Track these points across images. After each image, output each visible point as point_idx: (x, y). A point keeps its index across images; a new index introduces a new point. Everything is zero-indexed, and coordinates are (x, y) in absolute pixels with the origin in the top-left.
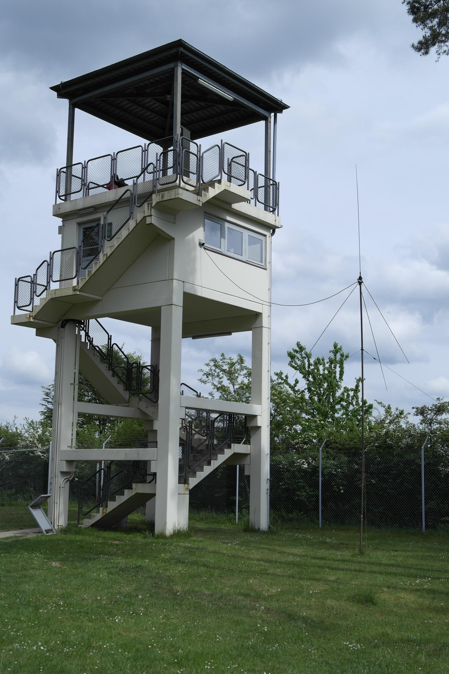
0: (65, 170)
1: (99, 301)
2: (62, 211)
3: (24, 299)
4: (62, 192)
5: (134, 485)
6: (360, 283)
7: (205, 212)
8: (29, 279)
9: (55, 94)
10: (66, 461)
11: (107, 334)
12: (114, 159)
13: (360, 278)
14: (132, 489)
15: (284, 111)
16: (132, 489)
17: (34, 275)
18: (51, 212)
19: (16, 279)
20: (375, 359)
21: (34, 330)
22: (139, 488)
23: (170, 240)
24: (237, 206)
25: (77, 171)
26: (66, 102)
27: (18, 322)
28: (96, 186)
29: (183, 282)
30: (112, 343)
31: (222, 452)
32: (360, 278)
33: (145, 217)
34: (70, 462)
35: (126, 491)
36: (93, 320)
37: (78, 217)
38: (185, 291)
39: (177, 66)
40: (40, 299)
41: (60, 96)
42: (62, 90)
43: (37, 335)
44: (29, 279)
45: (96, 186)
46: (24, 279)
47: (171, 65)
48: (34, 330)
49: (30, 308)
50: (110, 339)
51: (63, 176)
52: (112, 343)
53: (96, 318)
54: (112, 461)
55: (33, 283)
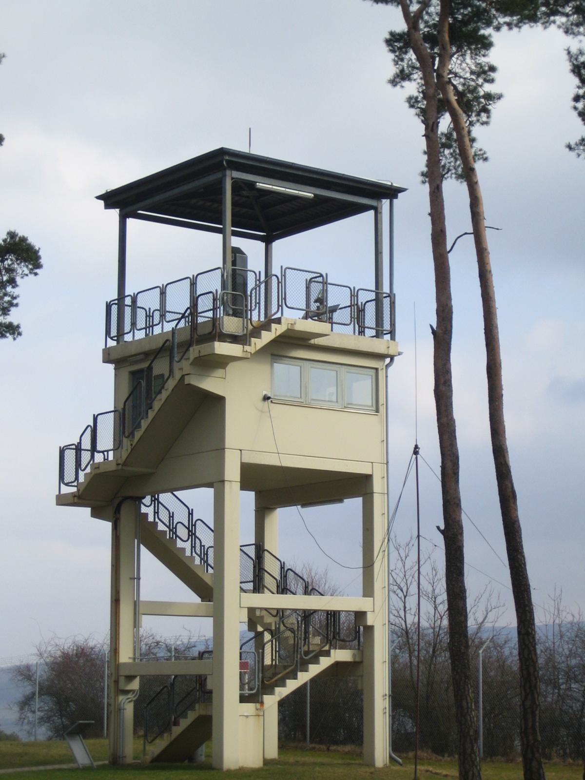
1: (152, 474)
2: (114, 356)
3: (69, 476)
4: (114, 332)
7: (272, 355)
8: (74, 447)
11: (166, 511)
12: (163, 293)
13: (416, 447)
14: (195, 710)
15: (400, 195)
17: (78, 443)
18: (100, 356)
19: (306, 280)
20: (435, 546)
21: (89, 509)
24: (312, 341)
26: (115, 213)
27: (62, 500)
30: (175, 522)
32: (416, 447)
33: (183, 376)
35: (189, 713)
36: (375, 333)
37: (131, 365)
38: (243, 461)
39: (225, 176)
41: (108, 206)
42: (111, 199)
46: (315, 279)
48: (89, 509)
49: (75, 484)
51: (114, 309)
52: (175, 522)
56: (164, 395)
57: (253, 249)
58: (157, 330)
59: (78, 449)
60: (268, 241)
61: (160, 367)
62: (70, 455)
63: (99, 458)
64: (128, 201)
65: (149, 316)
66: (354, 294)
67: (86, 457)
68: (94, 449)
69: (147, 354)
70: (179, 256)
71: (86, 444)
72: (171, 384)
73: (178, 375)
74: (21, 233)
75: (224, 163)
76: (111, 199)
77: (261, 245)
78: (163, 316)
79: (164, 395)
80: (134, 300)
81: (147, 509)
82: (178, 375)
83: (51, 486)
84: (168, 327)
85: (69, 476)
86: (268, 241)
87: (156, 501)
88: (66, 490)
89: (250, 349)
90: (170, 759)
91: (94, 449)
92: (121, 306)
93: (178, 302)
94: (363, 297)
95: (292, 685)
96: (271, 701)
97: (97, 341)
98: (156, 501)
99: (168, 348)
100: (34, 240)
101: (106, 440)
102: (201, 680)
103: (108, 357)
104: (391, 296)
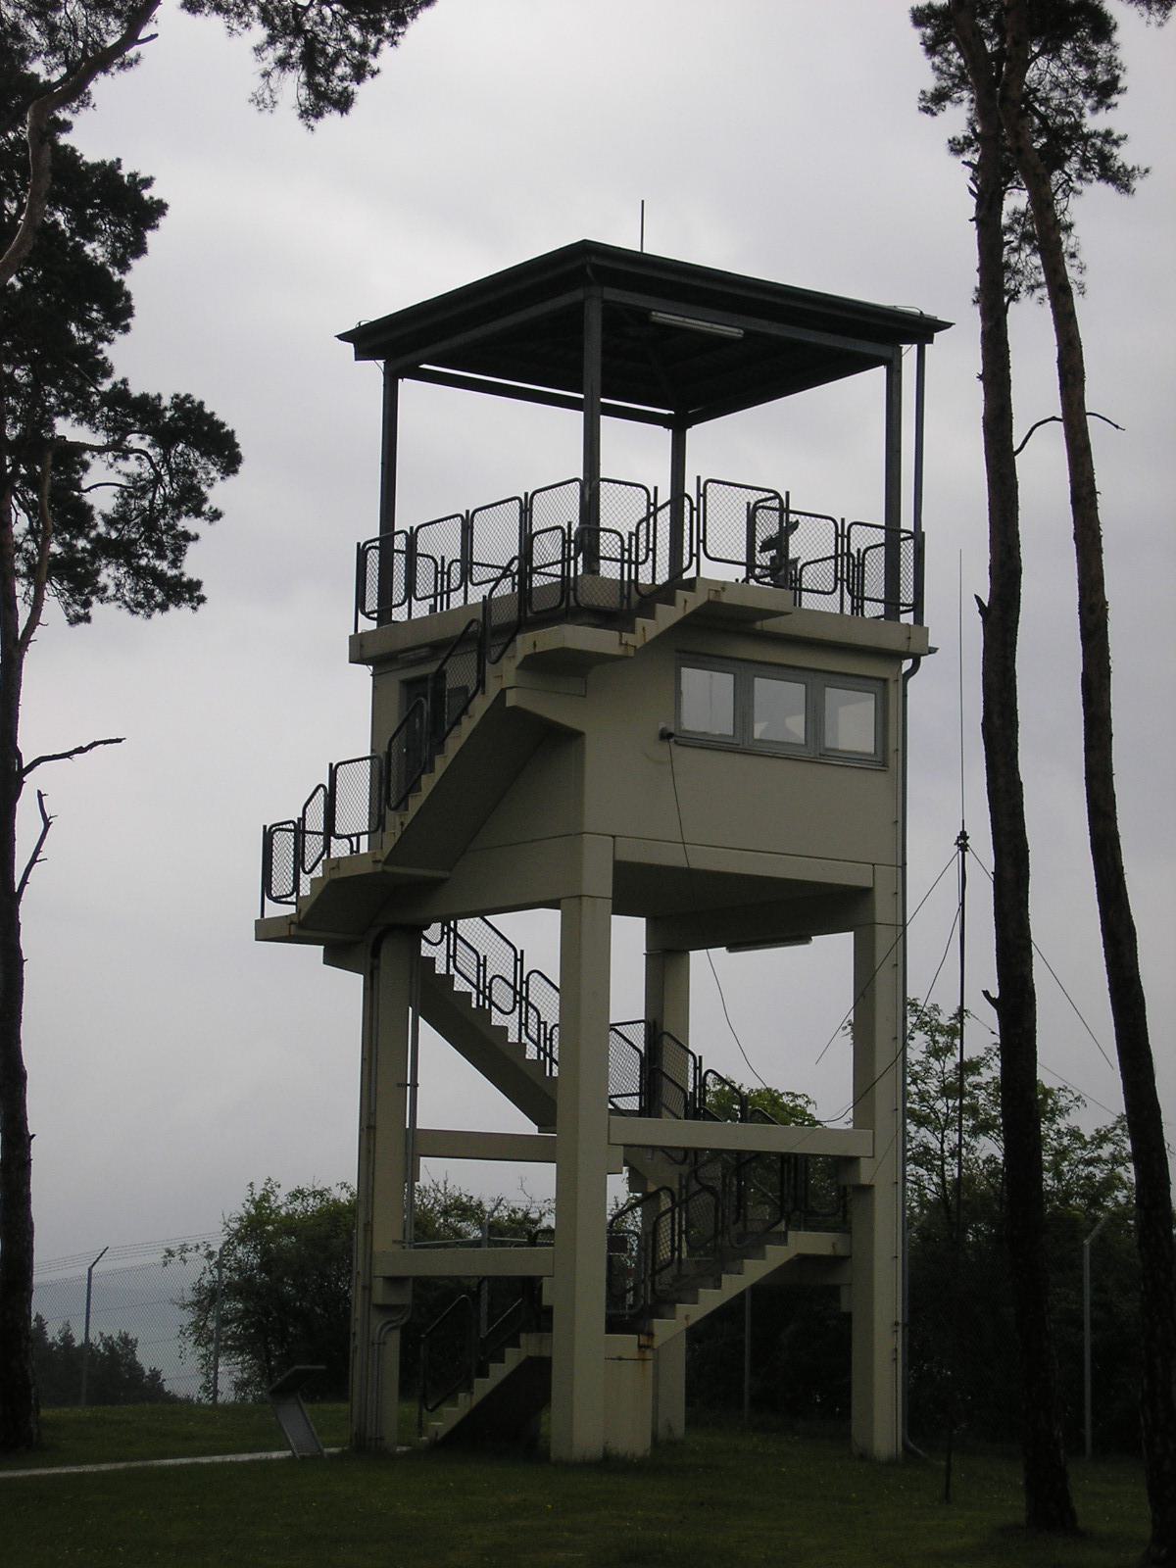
0: (377, 544)
1: (443, 881)
5: (523, 1338)
6: (964, 848)
9: (349, 348)
10: (384, 1277)
13: (963, 836)
14: (518, 1346)
16: (518, 1346)
22: (529, 1345)
23: (571, 737)
25: (400, 542)
26: (375, 369)
27: (268, 931)
28: (492, 584)
29: (614, 837)
31: (483, 1373)
32: (963, 836)
34: (394, 1281)
38: (618, 858)
40: (312, 880)
42: (367, 340)
43: (324, 963)
44: (291, 826)
45: (492, 584)
47: (578, 295)
49: (293, 899)
50: (519, 959)
51: (373, 557)
53: (481, 914)
54: (484, 1278)
55: (300, 830)
56: (468, 726)
58: (456, 600)
59: (300, 830)
60: (678, 427)
61: (460, 672)
62: (284, 843)
64: (404, 344)
65: (441, 572)
66: (842, 534)
67: (313, 845)
70: (498, 454)
71: (316, 821)
72: (480, 706)
73: (493, 689)
76: (367, 340)
77: (666, 435)
78: (466, 574)
79: (468, 726)
80: (412, 538)
82: (493, 689)
83: (247, 904)
85: (282, 883)
86: (678, 427)
87: (451, 933)
88: (274, 910)
89: (635, 640)
92: (387, 556)
93: (497, 544)
94: (860, 540)
95: (710, 1300)
96: (670, 1330)
97: (338, 618)
98: (451, 933)
99: (483, 634)
101: (355, 813)
104: (918, 537)
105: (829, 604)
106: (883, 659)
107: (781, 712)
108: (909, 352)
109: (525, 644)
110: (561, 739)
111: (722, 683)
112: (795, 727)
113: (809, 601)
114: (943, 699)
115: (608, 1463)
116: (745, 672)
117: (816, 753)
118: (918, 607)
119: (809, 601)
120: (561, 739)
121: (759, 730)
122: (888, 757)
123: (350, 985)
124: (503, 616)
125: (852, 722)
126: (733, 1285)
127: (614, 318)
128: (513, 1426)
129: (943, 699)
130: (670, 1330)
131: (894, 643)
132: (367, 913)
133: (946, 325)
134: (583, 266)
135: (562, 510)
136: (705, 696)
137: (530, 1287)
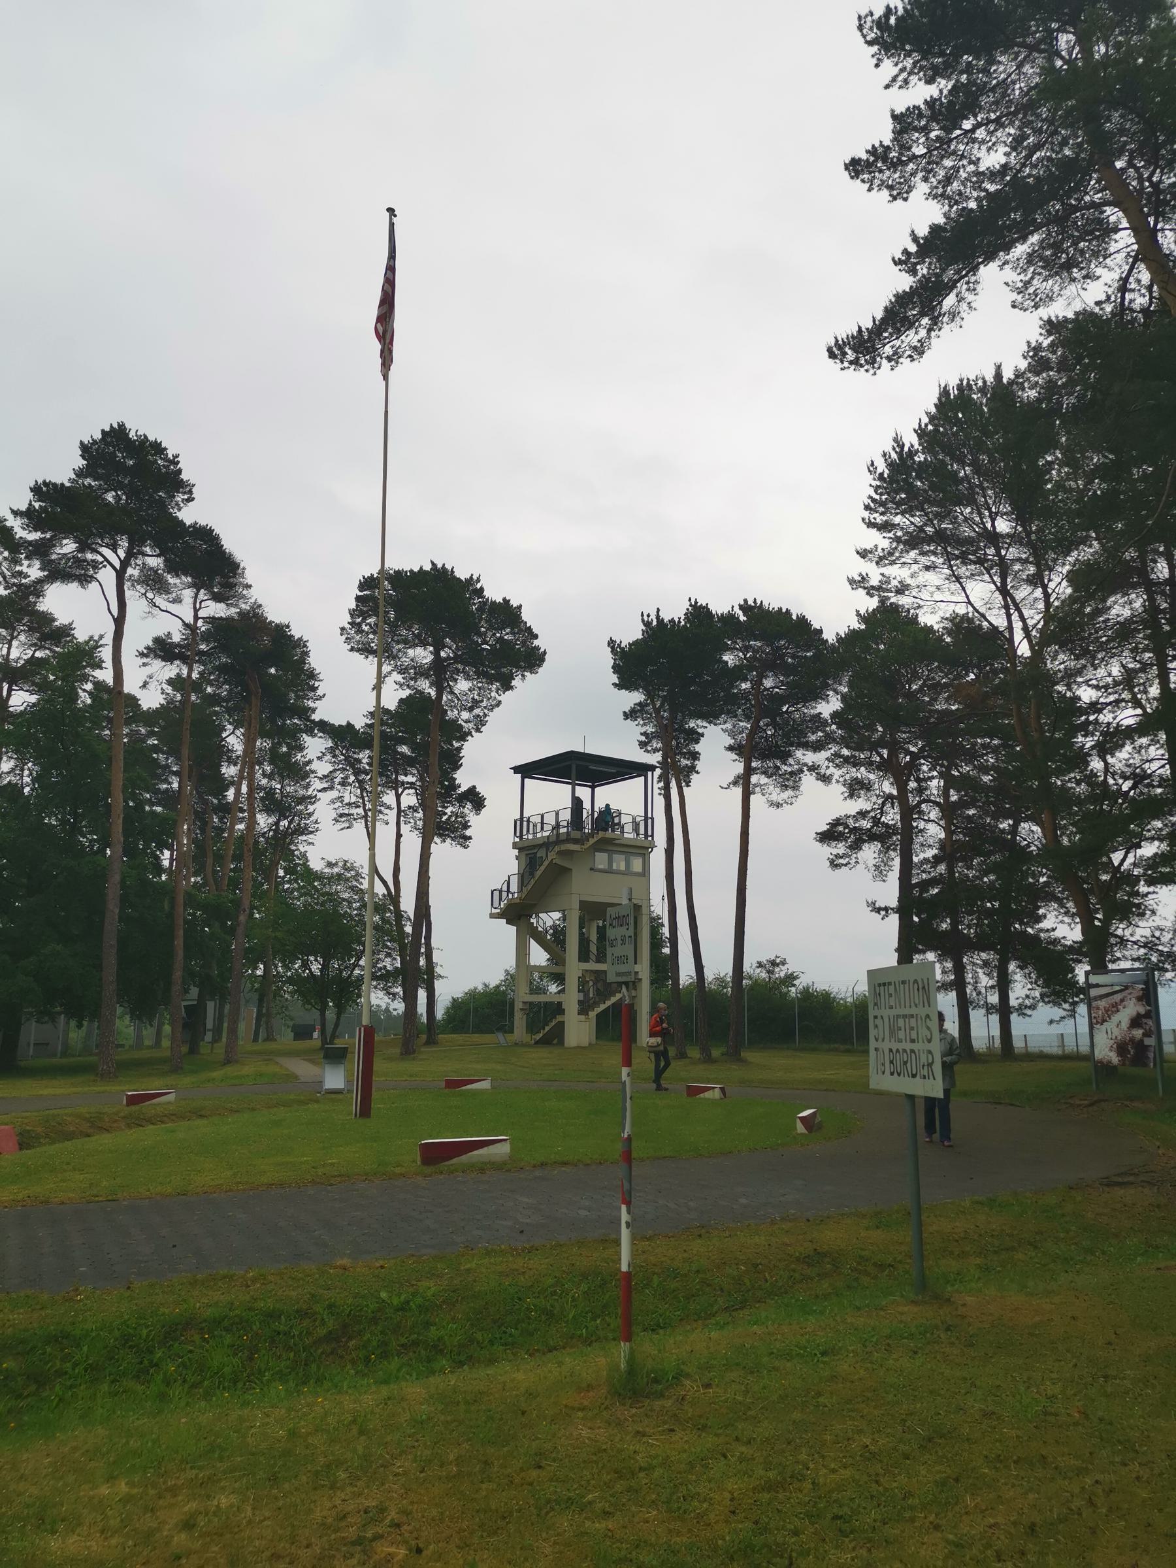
3: (496, 904)
22: (559, 1018)
27: (492, 916)
42: (517, 770)
56: (543, 868)
57: (583, 793)
58: (539, 835)
59: (501, 891)
60: (593, 788)
61: (541, 853)
62: (496, 894)
63: (510, 896)
64: (526, 771)
65: (535, 826)
66: (634, 818)
67: (504, 895)
68: (508, 891)
69: (534, 847)
70: (551, 800)
71: (505, 888)
72: (546, 863)
73: (550, 858)
74: (702, 602)
75: (1083, 718)
76: (517, 770)
77: (590, 790)
78: (542, 828)
79: (543, 868)
80: (528, 821)
81: (533, 921)
82: (550, 858)
83: (488, 909)
84: (546, 834)
85: (496, 904)
86: (593, 788)
87: (537, 916)
88: (494, 911)
89: (586, 846)
90: (546, 1042)
91: (508, 891)
92: (522, 822)
93: (550, 820)
94: (638, 819)
95: (603, 1007)
96: (592, 1014)
97: (510, 838)
98: (537, 916)
99: (547, 844)
100: (859, 377)
101: (514, 887)
102: (560, 1004)
103: (515, 846)
104: (652, 819)
105: (631, 836)
106: (643, 850)
107: (620, 863)
108: (650, 773)
109: (557, 849)
110: (567, 871)
111: (605, 856)
112: (623, 867)
113: (626, 835)
114: (657, 858)
115: (579, 1048)
116: (610, 853)
117: (628, 872)
118: (652, 836)
119: (626, 835)
120: (567, 871)
121: (614, 867)
122: (645, 873)
123: (513, 929)
124: (552, 839)
125: (637, 864)
126: (608, 1003)
127: (577, 766)
128: (555, 1038)
129: (657, 858)
130: (592, 1014)
131: (647, 845)
132: (516, 912)
133: (611, 643)
134: (571, 756)
135: (566, 816)
136: (601, 860)
137: (560, 1004)
